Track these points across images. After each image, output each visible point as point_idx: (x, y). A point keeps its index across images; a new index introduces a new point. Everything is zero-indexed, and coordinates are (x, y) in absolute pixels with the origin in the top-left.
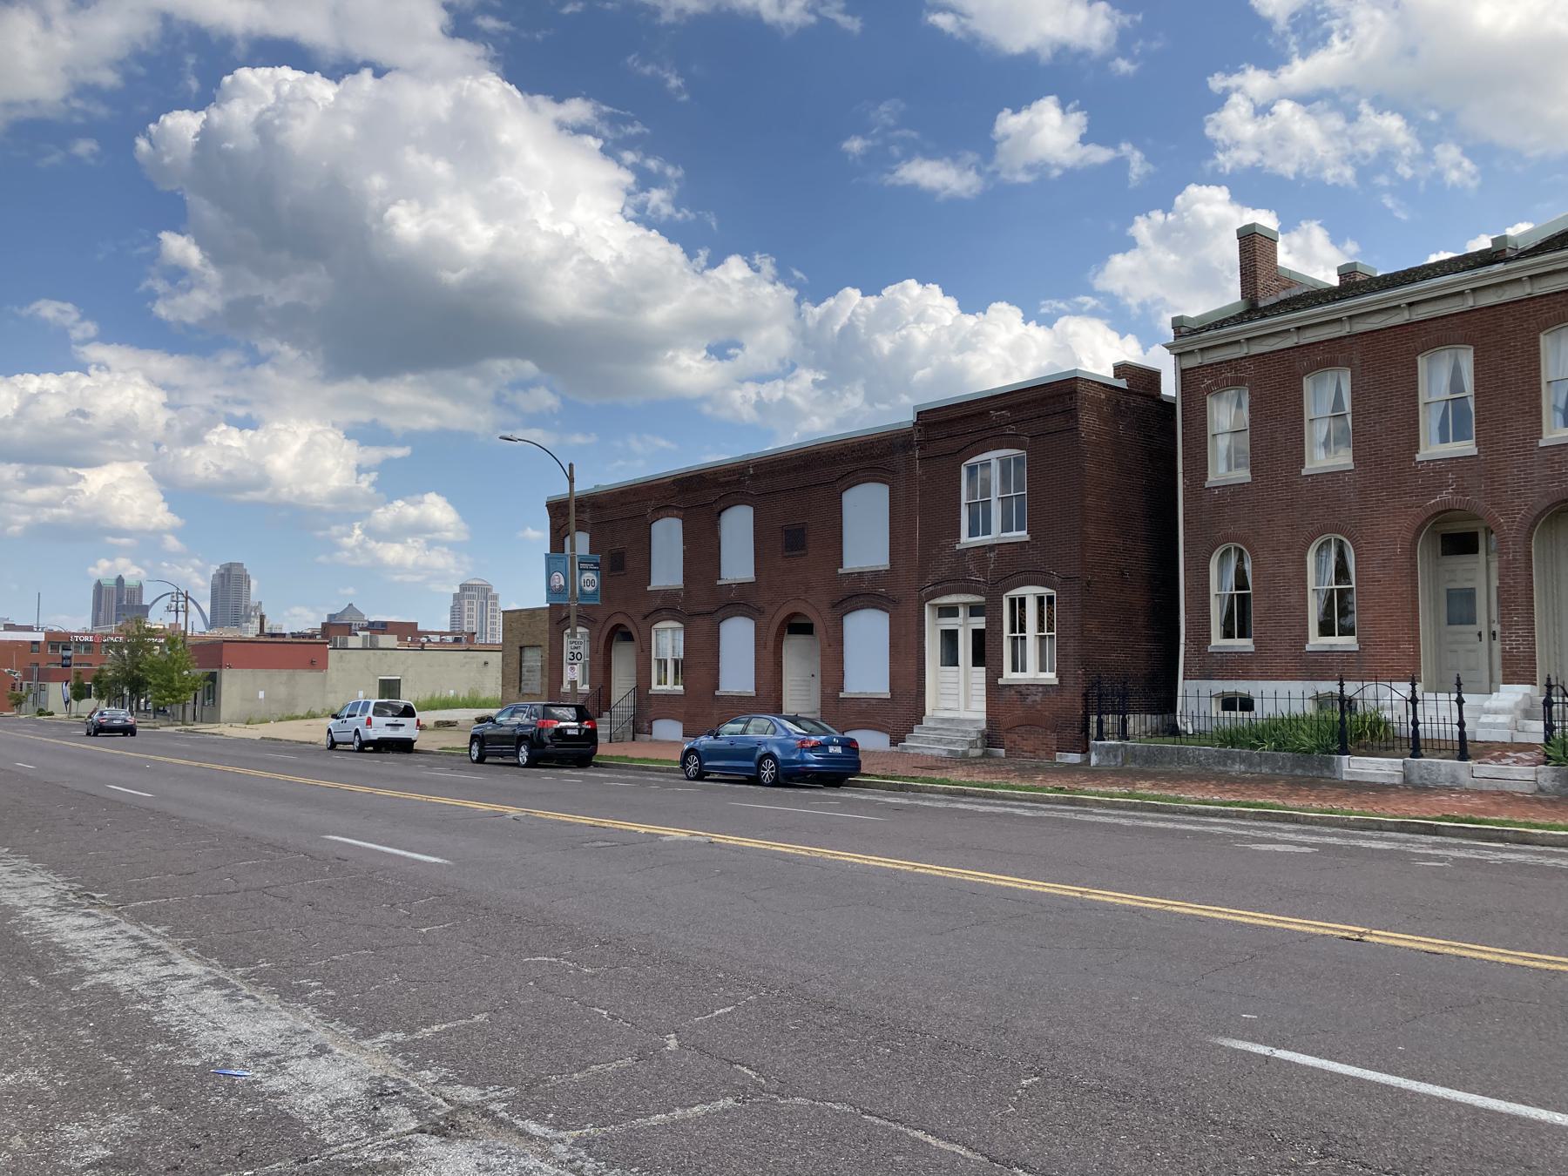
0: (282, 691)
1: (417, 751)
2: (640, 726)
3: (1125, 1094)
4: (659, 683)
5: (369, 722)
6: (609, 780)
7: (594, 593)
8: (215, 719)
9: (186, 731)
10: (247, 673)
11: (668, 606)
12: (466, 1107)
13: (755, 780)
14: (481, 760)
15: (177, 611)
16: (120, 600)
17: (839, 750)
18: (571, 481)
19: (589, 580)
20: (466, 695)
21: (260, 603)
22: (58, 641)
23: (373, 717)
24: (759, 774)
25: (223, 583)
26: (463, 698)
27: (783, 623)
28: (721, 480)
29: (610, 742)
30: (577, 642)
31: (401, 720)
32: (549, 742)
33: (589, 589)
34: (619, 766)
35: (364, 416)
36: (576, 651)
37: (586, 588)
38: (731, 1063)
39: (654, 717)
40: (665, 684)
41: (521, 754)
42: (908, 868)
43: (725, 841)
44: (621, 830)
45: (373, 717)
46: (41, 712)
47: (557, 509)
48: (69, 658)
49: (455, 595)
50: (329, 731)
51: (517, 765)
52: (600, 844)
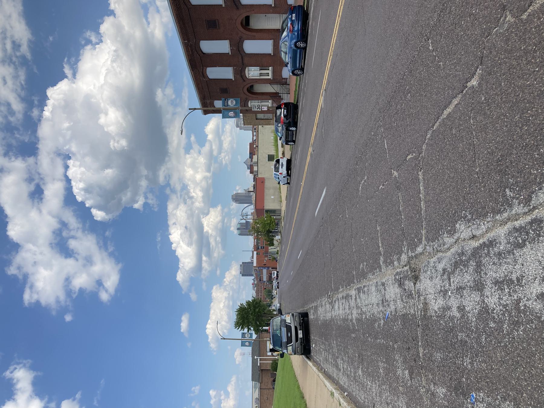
0: (272, 191)
1: (291, 158)
2: (284, 82)
3: (443, 5)
4: (268, 75)
5: (281, 174)
6: (302, 104)
7: (236, 101)
8: (280, 210)
9: (283, 219)
10: (265, 201)
11: (240, 72)
12: (409, 262)
13: (305, 49)
14: (294, 142)
15: (247, 215)
16: (244, 229)
17: (294, 15)
18: (195, 109)
19: (231, 103)
20: (273, 134)
21: (244, 190)
22: (256, 248)
23: (279, 172)
24: (302, 48)
25: (238, 201)
26: (274, 135)
27: (245, 29)
28: (191, 53)
29: (289, 93)
30: (253, 104)
31: (281, 164)
32: (288, 120)
33: (234, 102)
34: (298, 94)
35: (182, 151)
36: (257, 107)
37: (234, 104)
38: (406, 159)
39: (281, 78)
40: (269, 73)
41: (292, 130)
42: (339, 19)
43: (325, 85)
44: (319, 118)
45: (279, 172)
46: (278, 253)
47: (206, 112)
48: (261, 247)
49: (240, 129)
50: (283, 184)
51: (296, 131)
52: (323, 130)
